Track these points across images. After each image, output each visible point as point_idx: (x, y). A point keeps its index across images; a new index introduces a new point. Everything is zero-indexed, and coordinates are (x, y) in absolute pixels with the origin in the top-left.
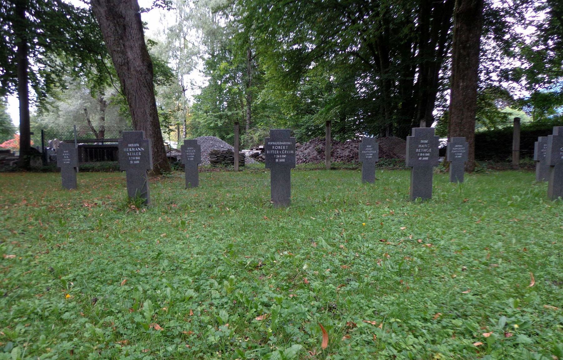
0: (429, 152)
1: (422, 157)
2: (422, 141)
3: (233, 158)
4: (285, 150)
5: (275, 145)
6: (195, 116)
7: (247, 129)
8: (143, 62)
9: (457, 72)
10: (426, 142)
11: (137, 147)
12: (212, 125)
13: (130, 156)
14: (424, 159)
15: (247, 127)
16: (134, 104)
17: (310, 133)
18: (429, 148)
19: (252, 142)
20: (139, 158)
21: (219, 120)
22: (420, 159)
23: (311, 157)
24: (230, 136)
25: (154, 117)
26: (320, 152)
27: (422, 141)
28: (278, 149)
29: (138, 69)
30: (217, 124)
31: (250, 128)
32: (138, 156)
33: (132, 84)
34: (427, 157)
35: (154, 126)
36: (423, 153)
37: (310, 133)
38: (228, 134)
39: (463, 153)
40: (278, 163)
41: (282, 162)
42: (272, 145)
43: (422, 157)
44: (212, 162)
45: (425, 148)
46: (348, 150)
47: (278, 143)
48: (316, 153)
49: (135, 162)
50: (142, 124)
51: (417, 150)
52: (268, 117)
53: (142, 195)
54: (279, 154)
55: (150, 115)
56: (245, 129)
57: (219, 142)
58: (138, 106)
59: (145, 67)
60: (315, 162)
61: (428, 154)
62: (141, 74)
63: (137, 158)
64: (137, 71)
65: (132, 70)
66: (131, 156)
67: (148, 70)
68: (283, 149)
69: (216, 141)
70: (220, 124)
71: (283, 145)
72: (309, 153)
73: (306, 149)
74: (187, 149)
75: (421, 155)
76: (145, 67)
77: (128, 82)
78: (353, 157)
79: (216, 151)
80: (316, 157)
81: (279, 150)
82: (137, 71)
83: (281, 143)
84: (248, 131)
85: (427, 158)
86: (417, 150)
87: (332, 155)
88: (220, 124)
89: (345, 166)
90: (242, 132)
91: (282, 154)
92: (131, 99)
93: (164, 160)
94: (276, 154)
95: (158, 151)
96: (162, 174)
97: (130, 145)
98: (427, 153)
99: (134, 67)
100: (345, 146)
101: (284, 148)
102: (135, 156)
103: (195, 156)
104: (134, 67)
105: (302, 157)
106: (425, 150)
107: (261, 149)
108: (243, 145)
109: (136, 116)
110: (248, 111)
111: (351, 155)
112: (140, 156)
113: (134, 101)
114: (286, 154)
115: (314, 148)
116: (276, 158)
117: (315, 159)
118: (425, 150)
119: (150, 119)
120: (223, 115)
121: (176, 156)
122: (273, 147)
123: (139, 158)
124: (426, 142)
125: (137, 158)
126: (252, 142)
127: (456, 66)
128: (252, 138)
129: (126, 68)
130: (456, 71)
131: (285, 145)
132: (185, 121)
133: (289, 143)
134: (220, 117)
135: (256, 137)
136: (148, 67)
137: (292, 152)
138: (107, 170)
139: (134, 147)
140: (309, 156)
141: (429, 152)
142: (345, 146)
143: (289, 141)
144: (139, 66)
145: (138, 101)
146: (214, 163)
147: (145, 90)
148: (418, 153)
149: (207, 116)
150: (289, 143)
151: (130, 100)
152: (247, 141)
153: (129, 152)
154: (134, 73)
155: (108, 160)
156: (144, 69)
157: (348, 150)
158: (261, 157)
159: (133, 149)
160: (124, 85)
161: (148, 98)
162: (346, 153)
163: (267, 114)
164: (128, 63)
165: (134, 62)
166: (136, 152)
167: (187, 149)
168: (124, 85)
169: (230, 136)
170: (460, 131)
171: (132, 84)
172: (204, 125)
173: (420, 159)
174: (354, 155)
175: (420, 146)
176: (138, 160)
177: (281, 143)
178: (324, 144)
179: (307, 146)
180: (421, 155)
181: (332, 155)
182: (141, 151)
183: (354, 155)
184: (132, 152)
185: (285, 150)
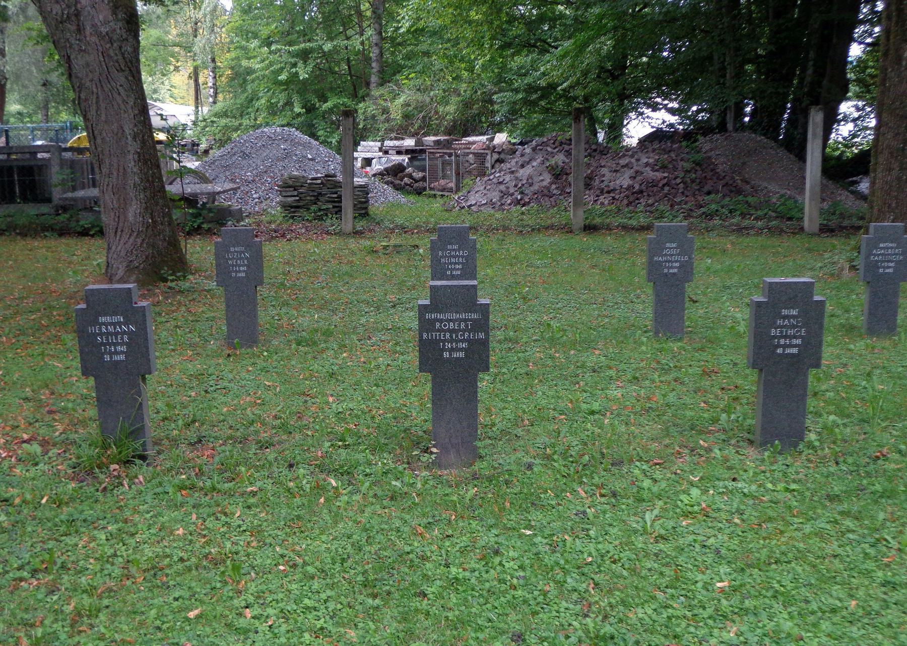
0: (801, 337)
1: (785, 346)
2: (785, 312)
3: (340, 197)
4: (464, 331)
5: (441, 321)
6: (239, 52)
7: (373, 85)
8: (114, 13)
9: (897, 23)
10: (794, 312)
11: (119, 324)
12: (283, 77)
13: (102, 344)
14: (788, 351)
15: (374, 79)
16: (93, 112)
17: (534, 96)
18: (801, 327)
19: (388, 120)
20: (124, 348)
21: (300, 64)
22: (780, 351)
23: (536, 187)
24: (329, 104)
25: (144, 142)
26: (558, 174)
27: (785, 312)
28: (449, 330)
29: (104, 30)
30: (297, 73)
31: (382, 83)
32: (121, 344)
33: (88, 65)
34: (795, 346)
35: (145, 163)
36: (786, 337)
37: (534, 96)
38: (326, 101)
39: (898, 262)
40: (449, 360)
41: (458, 359)
42: (437, 320)
43: (785, 346)
44: (285, 206)
45: (793, 327)
46: (629, 173)
47: (448, 316)
48: (547, 178)
49: (116, 358)
50: (115, 160)
51: (773, 330)
52: (427, 54)
53: (132, 433)
54: (451, 341)
55: (134, 138)
56: (368, 84)
57: (305, 146)
58: (103, 118)
59: (120, 24)
60: (546, 202)
61: (799, 341)
62: (111, 41)
63: (119, 348)
64: (100, 36)
65: (88, 33)
66: (105, 345)
67: (129, 30)
68: (460, 330)
69: (295, 143)
70: (303, 76)
71: (461, 320)
72: (530, 177)
73: (523, 166)
74: (228, 252)
75: (782, 342)
76: (120, 24)
77: (78, 62)
78: (641, 192)
79: (296, 178)
80: (548, 188)
81: (451, 331)
82: (100, 36)
83: (455, 316)
84: (375, 92)
85: (795, 351)
86: (773, 330)
87: (588, 186)
88: (303, 76)
89: (620, 220)
90: (361, 93)
91: (457, 342)
92: (86, 100)
93: (170, 243)
94: (444, 341)
95: (154, 222)
96: (165, 280)
97: (102, 319)
98: (795, 337)
99: (94, 26)
100: (623, 162)
101: (463, 326)
102: (115, 344)
103: (248, 266)
104: (94, 26)
105: (512, 190)
106: (791, 332)
107: (408, 152)
108: (365, 129)
109: (99, 141)
110: (375, 39)
111: (637, 187)
112: (127, 344)
113: (94, 107)
114: (468, 341)
115: (543, 163)
116: (444, 350)
117: (545, 193)
118: (791, 332)
119: (133, 147)
120: (311, 50)
121: (195, 195)
122: (438, 325)
123: (124, 348)
124: (794, 312)
125: (119, 348)
126: (388, 120)
127: (893, 8)
128: (385, 111)
129: (73, 28)
130: (894, 19)
131: (465, 320)
132: (213, 60)
133: (475, 316)
134: (304, 55)
135: (396, 108)
136: (128, 23)
137: (482, 336)
138: (27, 231)
139: (111, 324)
140: (531, 185)
141: (801, 337)
142: (623, 162)
143: (475, 312)
144: (106, 22)
145: (103, 106)
146: (292, 209)
147: (121, 79)
148: (775, 337)
149: (270, 53)
150: (475, 316)
151: (83, 104)
152: (374, 117)
153: (101, 334)
154: (94, 39)
155: (25, 200)
156: (119, 28)
157: (629, 173)
158: (410, 176)
159: (111, 329)
160: (70, 67)
161: (128, 96)
162: (624, 180)
163: (424, 47)
164: (77, 15)
165: (93, 12)
166: (116, 334)
167: (228, 252)
168: (70, 67)
169: (329, 104)
170: (901, 169)
171: (88, 65)
172: (264, 76)
173: (780, 351)
174: (643, 187)
175: (779, 322)
176: (122, 352)
177: (455, 316)
178: (568, 153)
179: (526, 159)
180: (782, 342)
181: (588, 186)
182: (130, 333)
183: (643, 187)
184: (108, 334)
185: (464, 331)
